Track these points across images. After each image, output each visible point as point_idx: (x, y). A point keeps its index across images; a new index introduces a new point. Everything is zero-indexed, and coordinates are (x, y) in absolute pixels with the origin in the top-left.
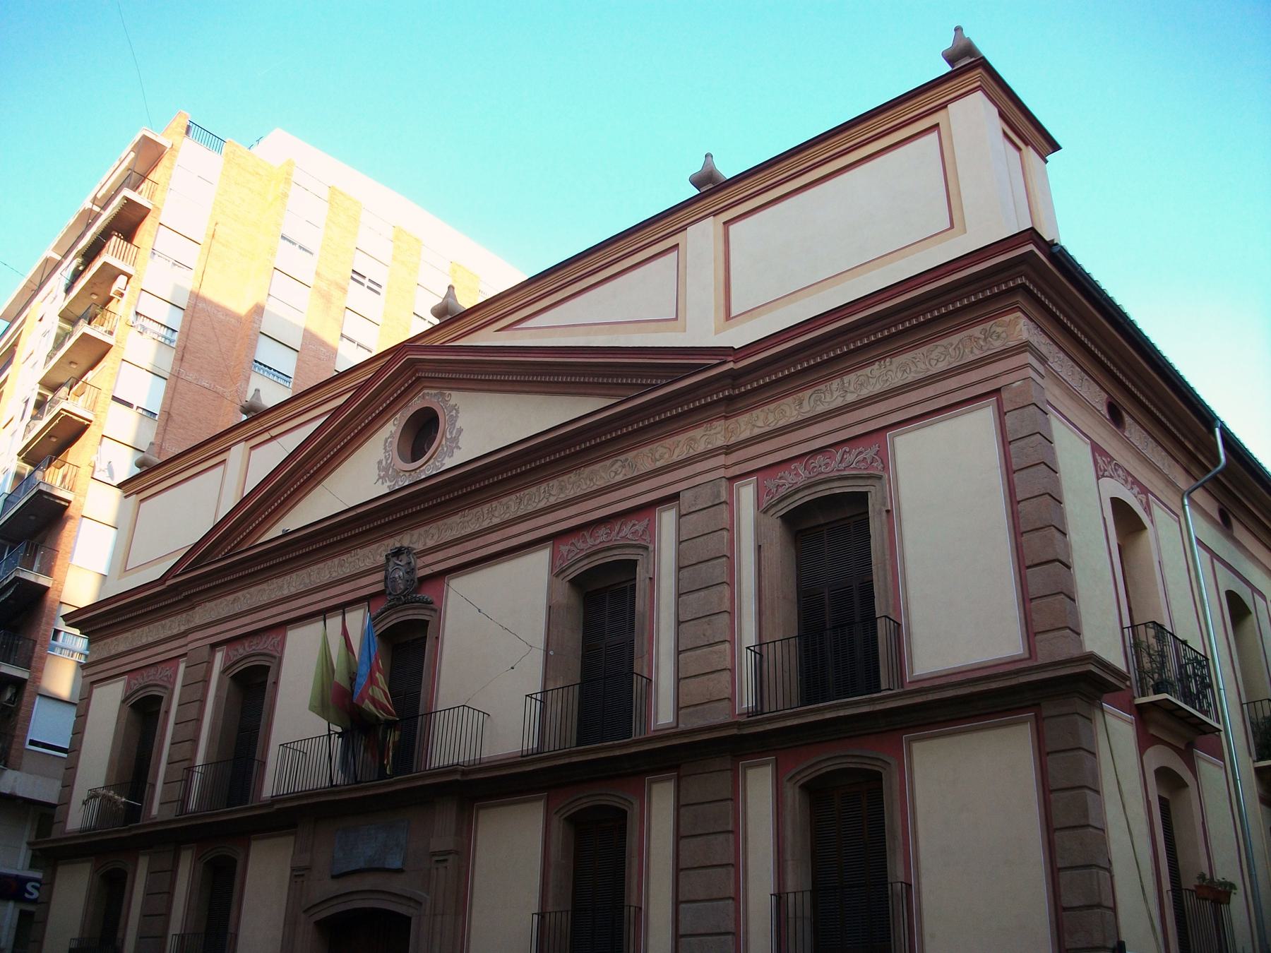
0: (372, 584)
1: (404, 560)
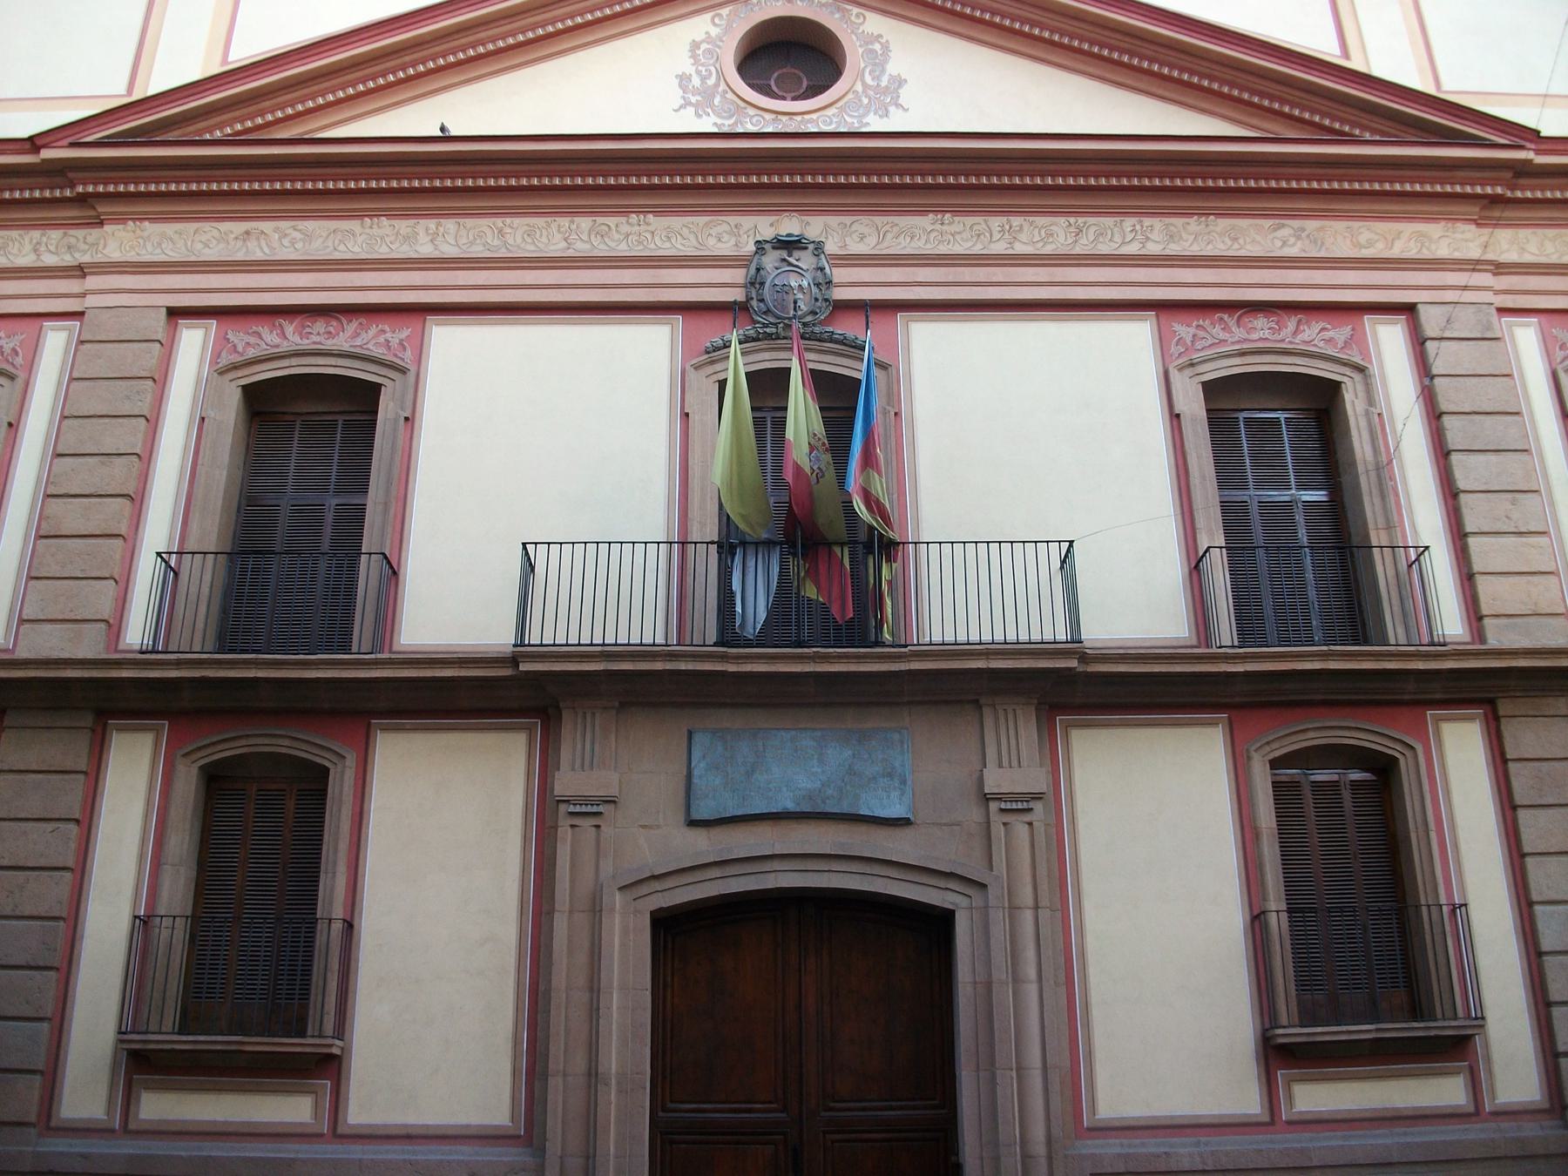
0: (726, 285)
1: (805, 260)
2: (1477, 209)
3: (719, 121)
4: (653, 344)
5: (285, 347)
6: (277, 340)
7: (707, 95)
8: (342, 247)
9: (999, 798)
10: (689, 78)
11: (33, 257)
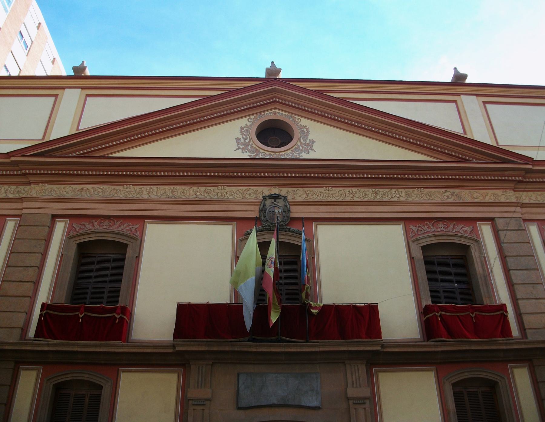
0: (252, 212)
1: (281, 203)
2: (513, 185)
3: (250, 154)
4: (225, 233)
5: (94, 230)
6: (91, 227)
7: (246, 145)
8: (116, 195)
9: (353, 399)
10: (240, 139)
11: (5, 195)
